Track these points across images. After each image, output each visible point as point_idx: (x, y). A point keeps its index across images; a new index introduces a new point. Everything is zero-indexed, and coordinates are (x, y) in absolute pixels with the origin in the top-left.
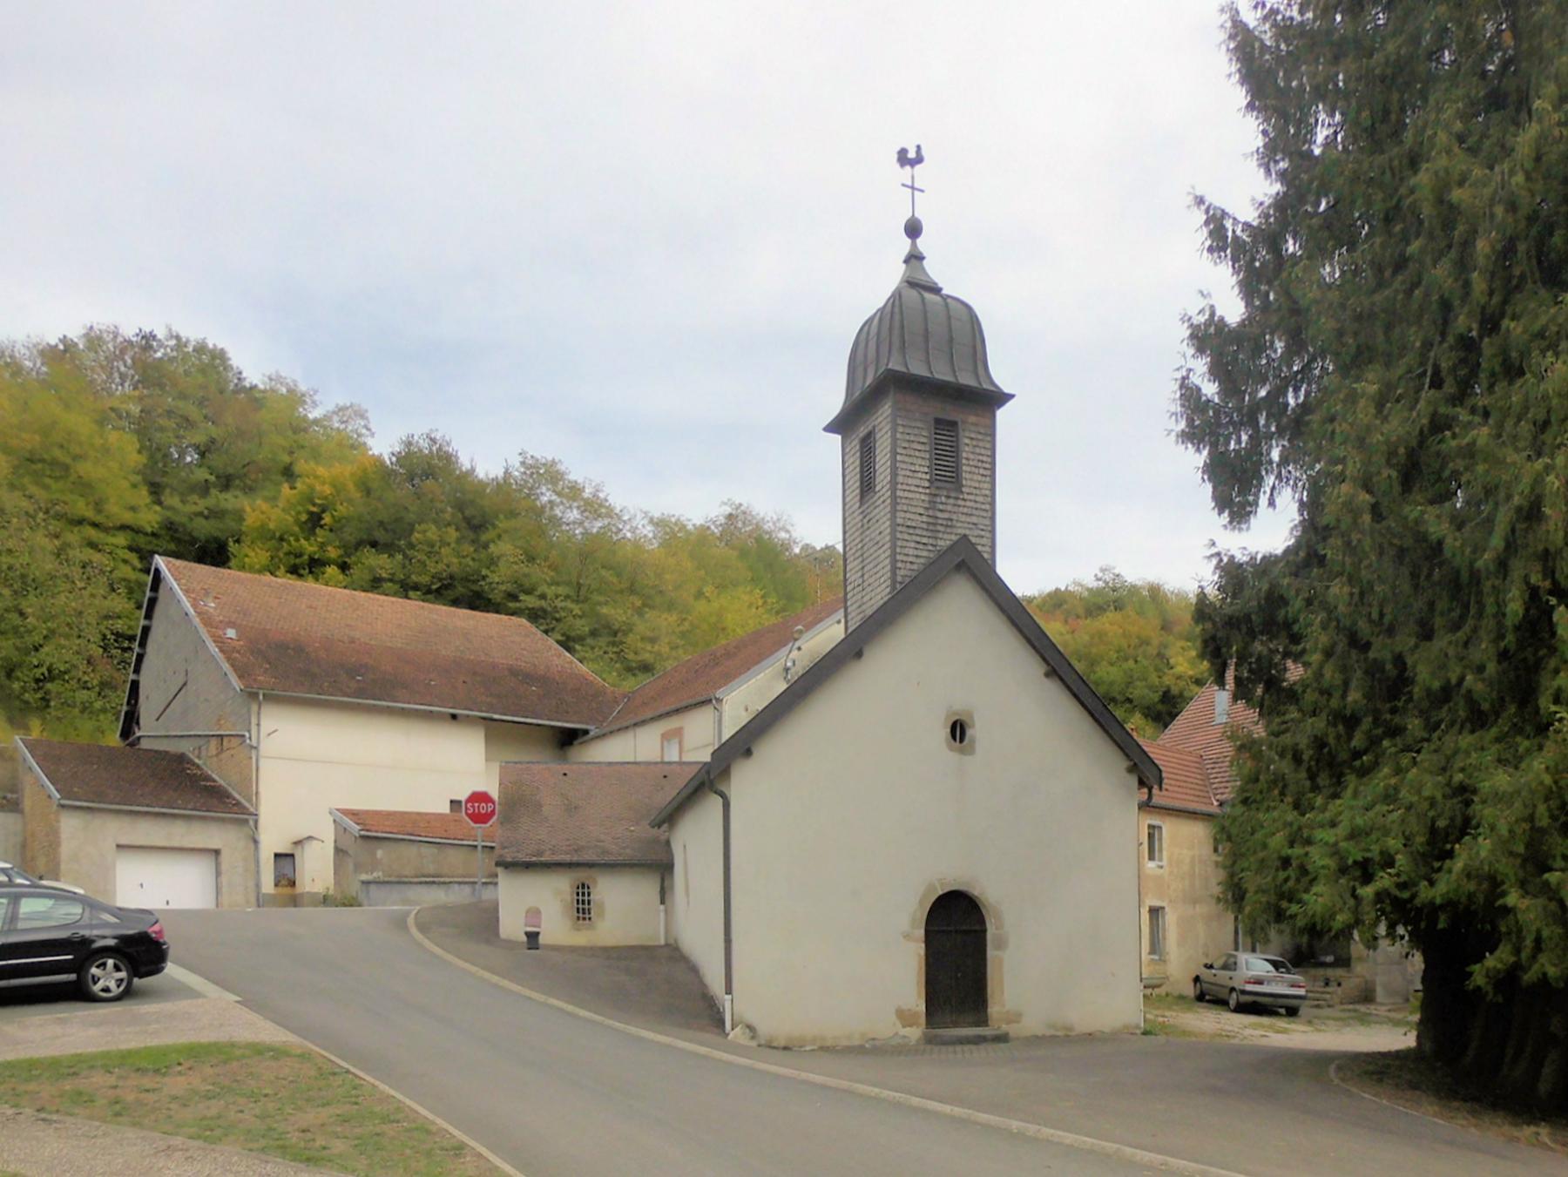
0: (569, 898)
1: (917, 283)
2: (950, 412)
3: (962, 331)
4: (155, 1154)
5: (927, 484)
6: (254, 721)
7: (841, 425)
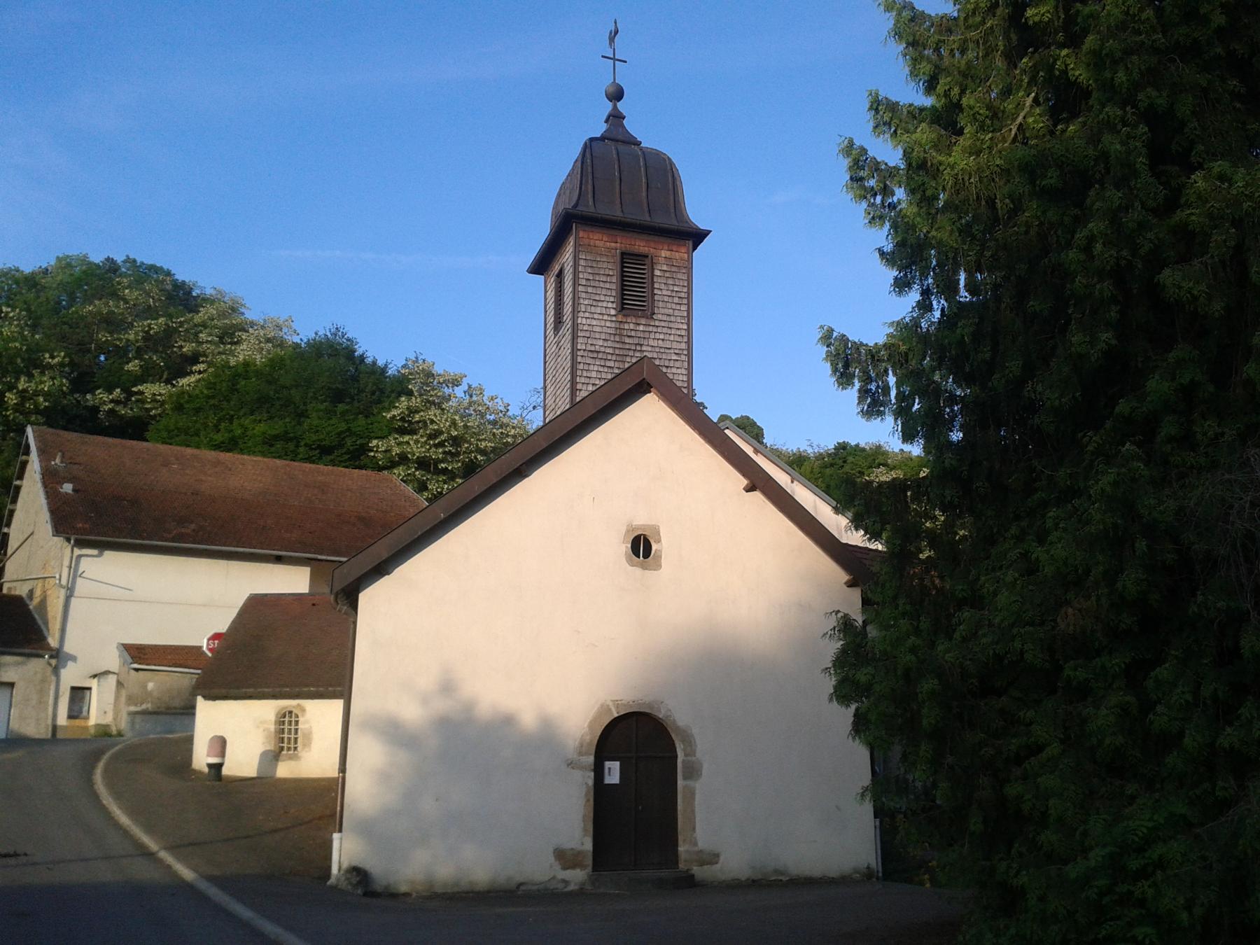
0: (272, 727)
1: (616, 135)
2: (640, 245)
3: (661, 176)
4: (1031, 724)
5: (613, 312)
6: (837, 524)
7: (541, 266)
